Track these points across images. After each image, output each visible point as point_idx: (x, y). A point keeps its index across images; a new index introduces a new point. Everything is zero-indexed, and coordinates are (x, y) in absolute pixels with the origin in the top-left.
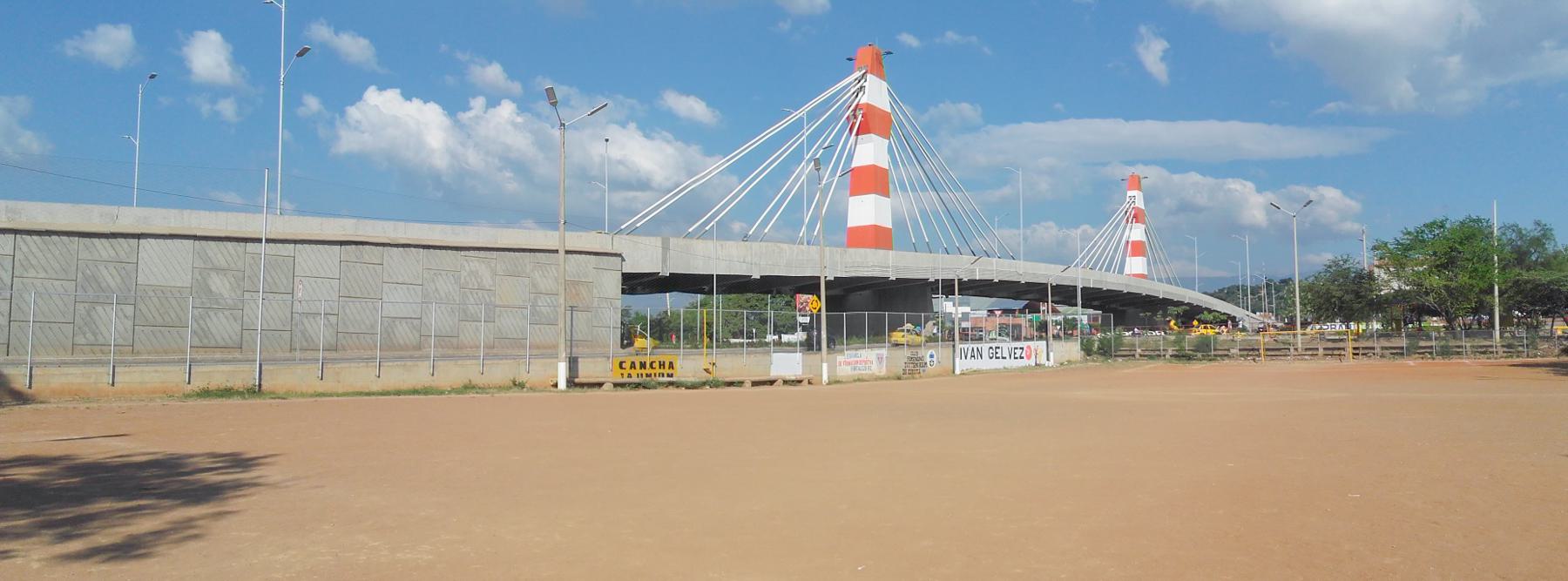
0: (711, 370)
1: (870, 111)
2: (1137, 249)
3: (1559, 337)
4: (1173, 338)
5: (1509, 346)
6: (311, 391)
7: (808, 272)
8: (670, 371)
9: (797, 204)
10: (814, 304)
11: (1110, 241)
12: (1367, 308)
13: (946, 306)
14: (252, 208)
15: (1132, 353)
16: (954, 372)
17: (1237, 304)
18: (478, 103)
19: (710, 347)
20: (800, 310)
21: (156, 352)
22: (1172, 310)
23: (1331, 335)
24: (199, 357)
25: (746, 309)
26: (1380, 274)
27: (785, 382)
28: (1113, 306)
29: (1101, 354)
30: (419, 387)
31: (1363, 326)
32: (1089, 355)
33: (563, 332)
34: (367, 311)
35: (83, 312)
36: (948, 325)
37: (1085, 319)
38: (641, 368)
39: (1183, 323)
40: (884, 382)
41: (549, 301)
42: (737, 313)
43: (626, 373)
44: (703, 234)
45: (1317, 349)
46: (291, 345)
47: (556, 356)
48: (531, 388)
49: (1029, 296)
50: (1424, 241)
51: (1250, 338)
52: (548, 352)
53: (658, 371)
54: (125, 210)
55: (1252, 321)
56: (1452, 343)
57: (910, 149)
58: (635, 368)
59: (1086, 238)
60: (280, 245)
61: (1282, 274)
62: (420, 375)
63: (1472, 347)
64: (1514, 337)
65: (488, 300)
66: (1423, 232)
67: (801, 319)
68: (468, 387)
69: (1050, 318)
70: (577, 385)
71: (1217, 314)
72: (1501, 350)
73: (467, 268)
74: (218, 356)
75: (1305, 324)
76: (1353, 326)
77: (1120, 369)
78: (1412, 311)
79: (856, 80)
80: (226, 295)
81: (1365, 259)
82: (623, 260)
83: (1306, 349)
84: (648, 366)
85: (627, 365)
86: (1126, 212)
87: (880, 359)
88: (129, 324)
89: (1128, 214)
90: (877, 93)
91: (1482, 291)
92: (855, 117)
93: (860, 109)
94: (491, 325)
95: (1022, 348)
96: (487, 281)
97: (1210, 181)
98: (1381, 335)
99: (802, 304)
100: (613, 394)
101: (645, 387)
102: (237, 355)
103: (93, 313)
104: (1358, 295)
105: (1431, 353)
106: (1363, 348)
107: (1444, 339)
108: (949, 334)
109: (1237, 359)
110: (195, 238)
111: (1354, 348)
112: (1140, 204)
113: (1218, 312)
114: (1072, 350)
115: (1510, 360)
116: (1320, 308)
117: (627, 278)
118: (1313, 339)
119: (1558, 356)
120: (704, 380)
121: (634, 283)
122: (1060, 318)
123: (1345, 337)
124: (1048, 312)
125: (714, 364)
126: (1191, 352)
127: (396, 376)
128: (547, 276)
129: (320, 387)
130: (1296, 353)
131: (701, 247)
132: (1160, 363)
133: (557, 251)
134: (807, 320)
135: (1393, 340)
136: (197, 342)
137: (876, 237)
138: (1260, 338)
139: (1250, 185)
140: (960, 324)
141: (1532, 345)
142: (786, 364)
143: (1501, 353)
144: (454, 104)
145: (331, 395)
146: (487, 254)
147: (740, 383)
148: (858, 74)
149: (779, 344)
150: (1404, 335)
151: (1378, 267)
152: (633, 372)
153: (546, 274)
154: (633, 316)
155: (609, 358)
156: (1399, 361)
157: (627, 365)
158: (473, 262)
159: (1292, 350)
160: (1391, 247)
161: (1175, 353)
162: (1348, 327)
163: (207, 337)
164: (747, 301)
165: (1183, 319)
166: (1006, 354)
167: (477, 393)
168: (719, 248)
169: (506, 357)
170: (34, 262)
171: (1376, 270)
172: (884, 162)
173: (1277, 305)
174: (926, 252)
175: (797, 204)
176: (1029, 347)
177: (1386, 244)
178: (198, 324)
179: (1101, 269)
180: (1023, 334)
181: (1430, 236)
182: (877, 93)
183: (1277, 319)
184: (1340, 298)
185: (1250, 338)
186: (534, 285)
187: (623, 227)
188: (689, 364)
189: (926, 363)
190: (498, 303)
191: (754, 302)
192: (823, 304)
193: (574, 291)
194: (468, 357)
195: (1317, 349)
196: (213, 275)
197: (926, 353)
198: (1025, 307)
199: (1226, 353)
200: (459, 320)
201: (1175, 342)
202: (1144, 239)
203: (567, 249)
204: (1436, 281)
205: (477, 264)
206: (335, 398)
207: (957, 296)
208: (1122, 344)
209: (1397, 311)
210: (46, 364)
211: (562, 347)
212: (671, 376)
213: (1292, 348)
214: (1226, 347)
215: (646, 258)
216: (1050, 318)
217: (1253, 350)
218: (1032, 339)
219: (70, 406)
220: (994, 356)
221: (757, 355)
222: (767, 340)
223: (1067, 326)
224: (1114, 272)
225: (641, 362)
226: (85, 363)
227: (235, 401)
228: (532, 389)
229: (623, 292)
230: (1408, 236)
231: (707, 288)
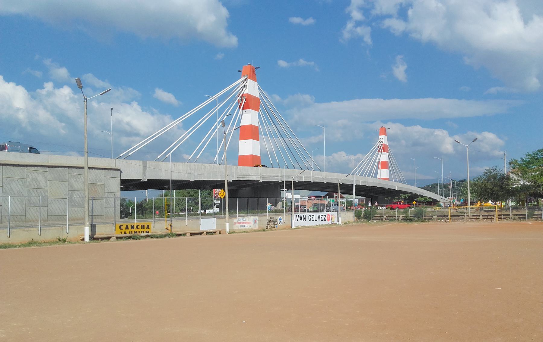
0: (169, 228)
1: (249, 98)
2: (384, 165)
7: (219, 178)
8: (148, 230)
9: (213, 145)
10: (222, 194)
11: (370, 161)
12: (506, 194)
13: (288, 195)
15: (381, 218)
16: (292, 228)
19: (168, 216)
20: (215, 197)
22: (402, 196)
23: (487, 208)
25: (187, 197)
26: (514, 177)
27: (208, 233)
28: (372, 194)
29: (365, 218)
31: (504, 204)
32: (359, 219)
33: (87, 211)
36: (289, 204)
37: (357, 201)
38: (131, 229)
39: (408, 203)
40: (257, 233)
41: (80, 194)
42: (183, 199)
43: (123, 231)
44: (165, 159)
47: (83, 224)
49: (329, 190)
50: (538, 159)
51: (443, 210)
52: (79, 222)
53: (141, 230)
55: (444, 201)
58: (128, 229)
59: (358, 161)
61: (459, 177)
65: (43, 194)
66: (537, 154)
67: (215, 202)
68: (32, 243)
71: (426, 198)
75: (472, 203)
78: (531, 195)
79: (242, 81)
81: (505, 169)
82: (121, 172)
83: (473, 216)
84: (135, 227)
85: (124, 227)
86: (378, 146)
87: (255, 221)
89: (379, 147)
92: (242, 101)
93: (244, 96)
94: (45, 208)
95: (325, 215)
96: (43, 184)
97: (426, 130)
98: (514, 208)
99: (216, 194)
100: (117, 242)
101: (133, 239)
104: (501, 187)
105: (541, 218)
106: (504, 215)
108: (288, 209)
109: (436, 221)
111: (499, 215)
112: (386, 142)
113: (427, 197)
114: (350, 216)
116: (480, 195)
118: (477, 210)
120: (165, 233)
122: (344, 200)
123: (494, 209)
124: (338, 198)
125: (171, 225)
126: (412, 217)
130: (468, 218)
131: (164, 165)
132: (396, 223)
133: (83, 168)
134: (219, 202)
138: (449, 210)
139: (445, 132)
140: (294, 204)
146: (43, 169)
147: (184, 234)
148: (243, 79)
149: (204, 214)
150: (526, 208)
151: (513, 173)
152: (127, 231)
153: (78, 180)
155: (114, 224)
156: (523, 222)
157: (124, 227)
158: (34, 174)
159: (466, 216)
160: (520, 163)
161: (403, 218)
162: (496, 204)
165: (408, 201)
166: (317, 219)
167: (37, 246)
168: (173, 166)
169: (54, 225)
171: (511, 174)
172: (256, 123)
173: (458, 193)
174: (277, 168)
175: (213, 145)
176: (328, 215)
177: (517, 160)
179: (365, 176)
181: (541, 156)
183: (458, 201)
184: (491, 189)
185: (443, 210)
186: (71, 186)
187: (121, 155)
189: (278, 223)
191: (192, 194)
192: (227, 193)
193: (94, 189)
194: (31, 226)
197: (278, 218)
198: (326, 195)
199: (430, 218)
201: (404, 212)
202: (388, 160)
203: (88, 166)
205: (36, 175)
207: (293, 190)
209: (523, 196)
211: (87, 219)
212: (148, 232)
213: (465, 215)
214: (431, 215)
216: (340, 200)
217: (445, 216)
221: (193, 220)
222: (198, 213)
223: (348, 205)
224: (372, 177)
225: (131, 226)
228: (70, 242)
229: (122, 189)
230: (529, 157)
231: (167, 187)
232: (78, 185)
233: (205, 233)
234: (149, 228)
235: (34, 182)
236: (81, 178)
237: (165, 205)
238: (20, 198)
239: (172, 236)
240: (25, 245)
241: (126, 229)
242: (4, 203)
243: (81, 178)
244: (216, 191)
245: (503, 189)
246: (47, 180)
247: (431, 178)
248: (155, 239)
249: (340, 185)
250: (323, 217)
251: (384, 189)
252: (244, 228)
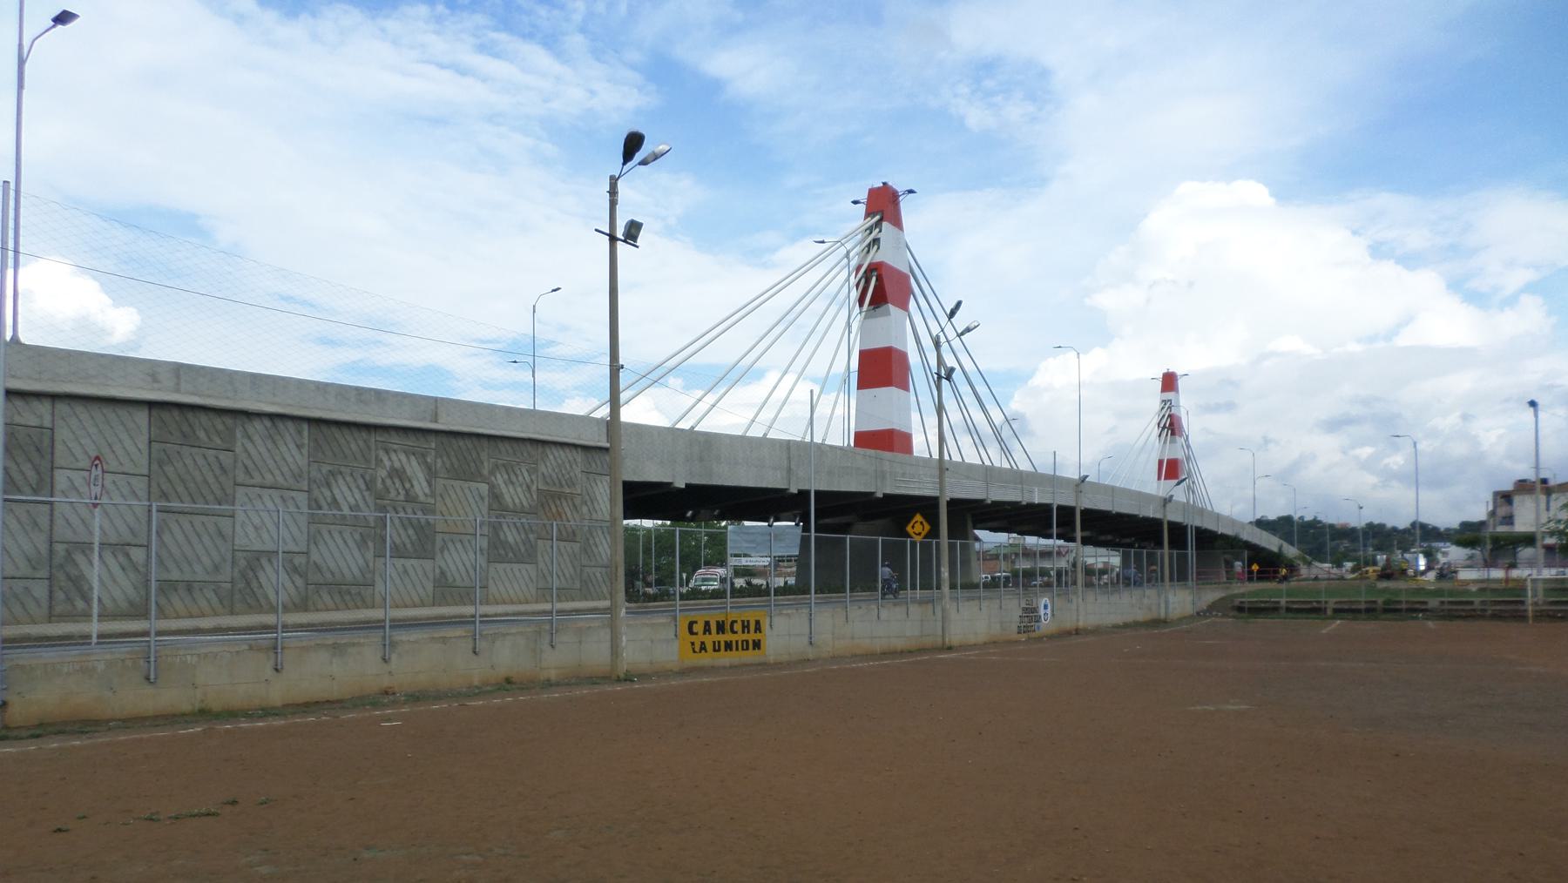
34: (206, 539)
46: (50, 607)
73: (387, 463)
84: (728, 627)
85: (699, 628)
117: (630, 488)
153: (514, 478)
157: (699, 628)
193: (554, 510)
200: (375, 556)
205: (403, 457)
234: (760, 632)
235: (397, 481)
236: (513, 471)
238: (360, 530)
241: (704, 633)
242: (313, 546)
243: (513, 471)
246: (431, 474)
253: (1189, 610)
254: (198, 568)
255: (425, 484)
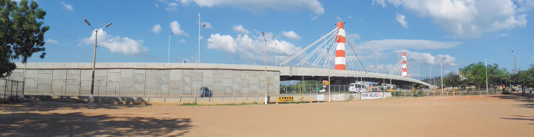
1: (340, 37)
2: (405, 70)
3: (501, 90)
4: (413, 91)
5: (490, 92)
6: (207, 104)
7: (326, 75)
8: (292, 99)
10: (327, 83)
14: (194, 61)
17: (428, 83)
18: (239, 36)
20: (324, 84)
21: (174, 95)
22: (413, 84)
24: (182, 96)
27: (320, 102)
28: (399, 84)
30: (232, 103)
31: (457, 88)
35: (159, 86)
43: (281, 100)
44: (300, 66)
45: (447, 93)
48: (259, 104)
49: (379, 82)
52: (262, 95)
53: (289, 99)
54: (167, 63)
56: (477, 92)
57: (350, 45)
60: (199, 70)
61: (438, 76)
62: (232, 100)
63: (482, 92)
64: (491, 90)
67: (324, 86)
68: (244, 104)
69: (384, 87)
70: (269, 103)
72: (488, 93)
74: (186, 96)
75: (444, 88)
76: (455, 88)
77: (401, 99)
80: (188, 82)
81: (457, 72)
82: (280, 73)
83: (444, 94)
84: (287, 98)
85: (281, 98)
87: (343, 96)
88: (168, 89)
90: (342, 33)
91: (484, 80)
95: (377, 94)
96: (248, 78)
97: (419, 53)
101: (286, 103)
102: (191, 96)
103: (161, 86)
104: (456, 81)
105: (472, 94)
106: (457, 93)
107: (476, 91)
110: (181, 69)
111: (455, 93)
112: (405, 59)
114: (389, 94)
115: (490, 95)
116: (447, 84)
117: (281, 77)
118: (446, 91)
119: (501, 94)
120: (300, 101)
121: (283, 78)
127: (227, 101)
128: (262, 77)
129: (209, 103)
132: (410, 97)
133: (265, 71)
134: (325, 87)
135: (464, 91)
136: (182, 93)
137: (342, 67)
138: (433, 91)
141: (495, 92)
142: (320, 97)
143: (488, 94)
144: (234, 35)
145: (211, 105)
147: (309, 102)
148: (337, 28)
151: (460, 74)
152: (283, 100)
154: (283, 86)
156: (465, 96)
157: (281, 98)
162: (453, 88)
163: (184, 91)
164: (311, 82)
165: (416, 87)
166: (374, 95)
169: (253, 96)
170: (149, 75)
172: (344, 49)
176: (379, 94)
178: (182, 89)
180: (378, 91)
182: (342, 33)
184: (451, 81)
188: (297, 97)
190: (250, 83)
191: (313, 82)
194: (243, 96)
195: (447, 93)
196: (185, 77)
198: (378, 84)
204: (473, 77)
206: (212, 106)
207: (361, 81)
208: (401, 93)
209: (465, 84)
210: (152, 97)
211: (266, 94)
212: (292, 100)
215: (286, 72)
217: (432, 94)
218: (380, 92)
219: (156, 107)
220: (371, 96)
226: (159, 97)
227: (190, 106)
228: (259, 104)
229: (280, 80)
232: (262, 79)
233: (319, 102)
237: (300, 87)
239: (303, 103)
240: (240, 104)
244: (324, 81)
245: (456, 81)
247: (426, 76)
248: (295, 104)
249: (330, 78)
250: (377, 95)
251: (288, 77)
252: (337, 100)
253: (343, 99)
254: (219, 89)
255: (248, 77)
